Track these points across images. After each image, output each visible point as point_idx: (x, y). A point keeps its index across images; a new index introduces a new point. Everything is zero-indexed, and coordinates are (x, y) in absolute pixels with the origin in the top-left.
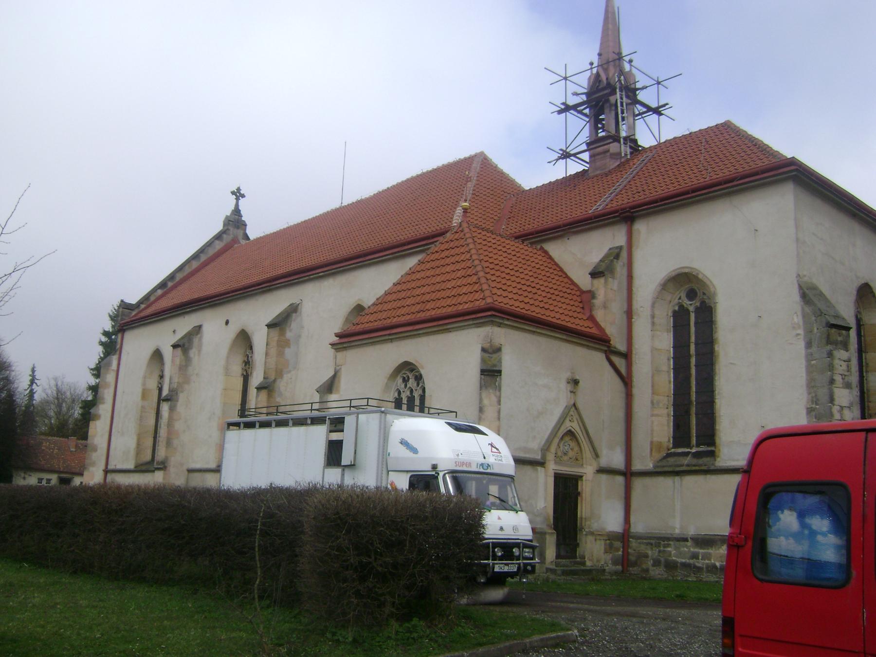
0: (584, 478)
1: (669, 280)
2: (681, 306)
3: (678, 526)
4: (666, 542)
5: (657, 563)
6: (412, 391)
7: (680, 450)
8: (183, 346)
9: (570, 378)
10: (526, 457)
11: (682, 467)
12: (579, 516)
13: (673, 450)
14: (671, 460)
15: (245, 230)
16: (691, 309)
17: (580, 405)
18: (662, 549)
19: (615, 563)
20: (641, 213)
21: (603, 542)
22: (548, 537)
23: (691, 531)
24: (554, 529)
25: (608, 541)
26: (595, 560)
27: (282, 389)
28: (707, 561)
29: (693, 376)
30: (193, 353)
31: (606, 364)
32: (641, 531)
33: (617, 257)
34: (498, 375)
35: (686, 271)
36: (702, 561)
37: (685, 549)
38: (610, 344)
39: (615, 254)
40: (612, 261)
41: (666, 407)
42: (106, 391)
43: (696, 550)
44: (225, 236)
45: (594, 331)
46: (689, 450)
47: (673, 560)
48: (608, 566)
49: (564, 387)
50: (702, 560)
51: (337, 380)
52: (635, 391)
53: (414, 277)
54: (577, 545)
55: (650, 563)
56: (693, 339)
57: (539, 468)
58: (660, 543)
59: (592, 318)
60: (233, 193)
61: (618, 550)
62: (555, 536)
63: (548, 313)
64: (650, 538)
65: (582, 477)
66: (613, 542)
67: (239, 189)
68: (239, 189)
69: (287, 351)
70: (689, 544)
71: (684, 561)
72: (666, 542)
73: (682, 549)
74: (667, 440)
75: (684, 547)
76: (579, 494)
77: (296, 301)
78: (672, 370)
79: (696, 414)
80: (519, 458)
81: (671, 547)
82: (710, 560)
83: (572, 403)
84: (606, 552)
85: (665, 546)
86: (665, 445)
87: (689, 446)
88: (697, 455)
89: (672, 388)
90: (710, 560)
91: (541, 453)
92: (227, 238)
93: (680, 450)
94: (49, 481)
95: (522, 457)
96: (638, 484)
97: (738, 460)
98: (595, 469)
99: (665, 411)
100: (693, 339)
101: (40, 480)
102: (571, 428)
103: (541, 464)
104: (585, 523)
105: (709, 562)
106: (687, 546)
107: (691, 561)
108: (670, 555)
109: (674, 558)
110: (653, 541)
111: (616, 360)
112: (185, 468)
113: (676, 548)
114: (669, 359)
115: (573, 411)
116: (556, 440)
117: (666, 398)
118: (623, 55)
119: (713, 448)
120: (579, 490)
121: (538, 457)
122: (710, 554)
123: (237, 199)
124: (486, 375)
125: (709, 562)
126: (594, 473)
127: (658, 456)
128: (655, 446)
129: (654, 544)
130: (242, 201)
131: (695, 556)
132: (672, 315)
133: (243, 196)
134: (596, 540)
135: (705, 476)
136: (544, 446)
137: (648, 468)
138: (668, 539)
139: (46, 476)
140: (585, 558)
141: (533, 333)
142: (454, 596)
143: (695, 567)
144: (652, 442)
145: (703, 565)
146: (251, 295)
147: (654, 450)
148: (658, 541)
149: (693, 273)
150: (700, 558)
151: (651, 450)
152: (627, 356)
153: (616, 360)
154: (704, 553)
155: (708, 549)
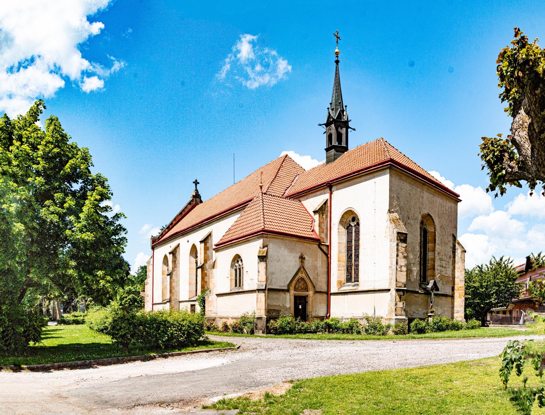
8: (174, 253)
15: (200, 198)
30: (177, 254)
31: (319, 250)
42: (150, 273)
44: (192, 202)
49: (298, 260)
53: (238, 223)
60: (194, 182)
68: (196, 180)
87: (351, 282)
96: (325, 296)
103: (288, 291)
112: (178, 300)
116: (294, 282)
121: (286, 288)
130: (198, 185)
133: (198, 183)
142: (76, 276)
146: (352, 179)
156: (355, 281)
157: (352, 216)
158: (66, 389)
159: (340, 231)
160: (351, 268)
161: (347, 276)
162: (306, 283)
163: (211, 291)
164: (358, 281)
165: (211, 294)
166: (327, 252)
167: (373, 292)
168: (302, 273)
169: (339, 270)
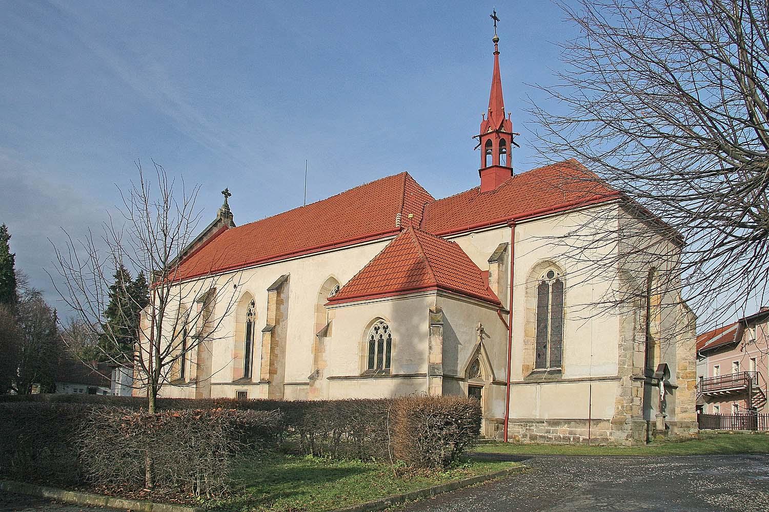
2: (544, 282)
6: (381, 336)
7: (540, 370)
13: (535, 370)
14: (535, 376)
16: (550, 283)
18: (528, 428)
23: (546, 417)
27: (280, 331)
33: (505, 250)
39: (503, 248)
40: (502, 253)
45: (490, 297)
56: (550, 302)
59: (488, 289)
63: (465, 286)
67: (227, 190)
69: (282, 307)
70: (545, 424)
71: (541, 434)
77: (286, 273)
86: (530, 367)
87: (545, 367)
88: (550, 373)
92: (220, 225)
93: (540, 370)
94: (81, 391)
97: (576, 375)
100: (550, 302)
101: (75, 390)
107: (546, 435)
118: (614, 386)
119: (560, 369)
123: (226, 197)
128: (526, 368)
131: (548, 432)
133: (230, 195)
139: (78, 387)
141: (459, 300)
152: (509, 313)
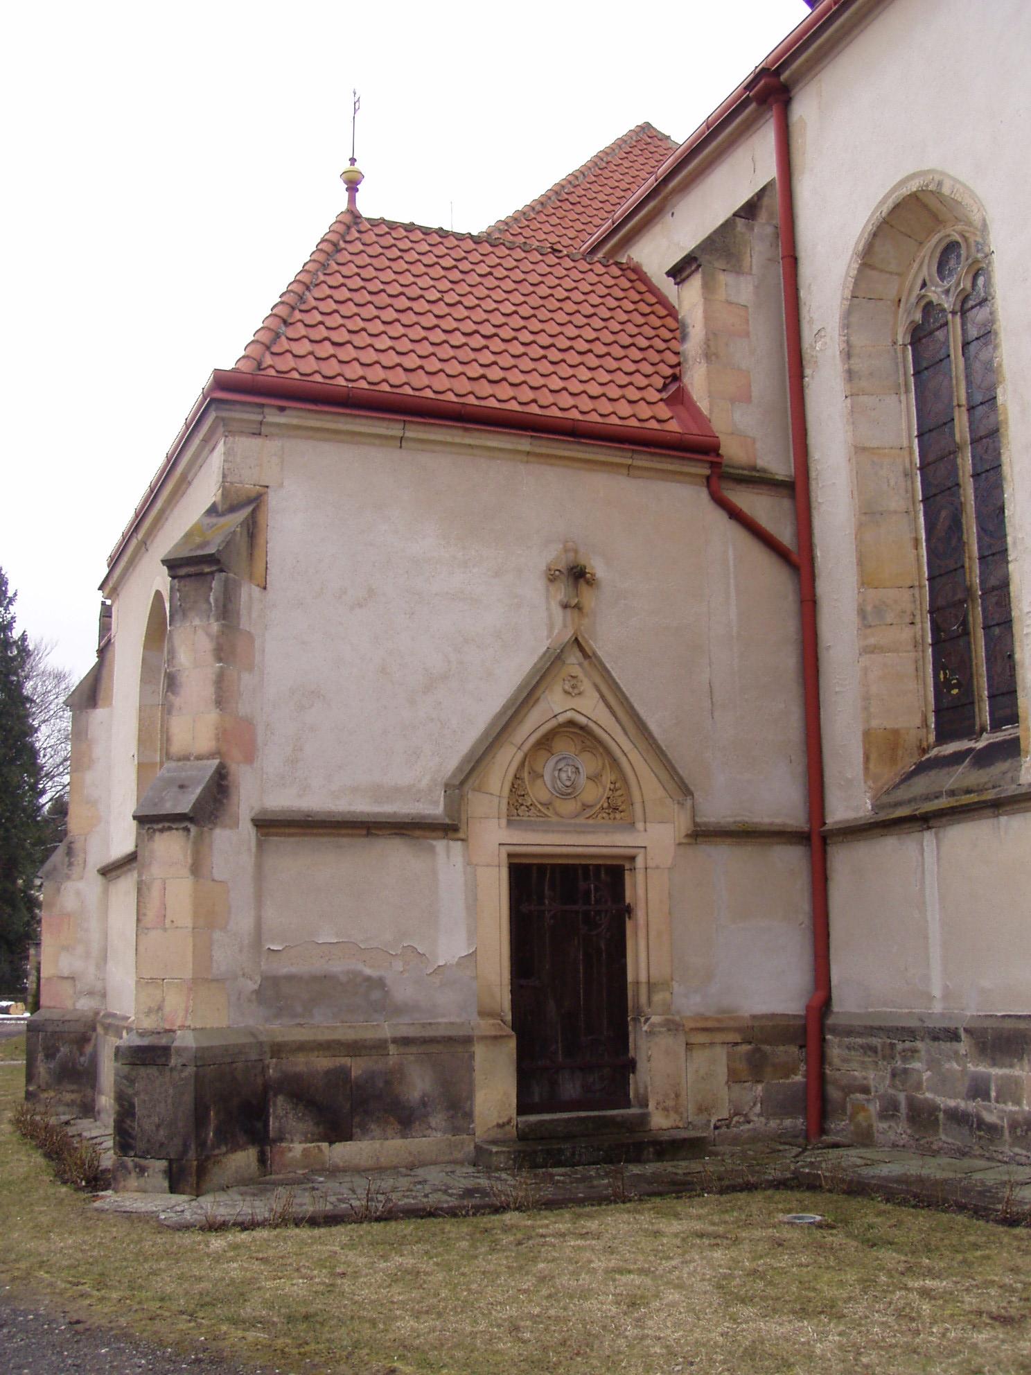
0: (640, 862)
1: (875, 235)
3: (937, 992)
4: (908, 1044)
5: (889, 1110)
9: (562, 566)
10: (378, 814)
11: (936, 801)
12: (630, 978)
17: (603, 647)
18: (899, 1064)
19: (778, 1106)
20: (794, 66)
21: (721, 1054)
22: (479, 1051)
23: (971, 1008)
24: (513, 1029)
25: (745, 1048)
26: (691, 1108)
28: (1011, 1107)
29: (968, 507)
31: (718, 517)
32: (854, 1010)
34: (212, 573)
35: (913, 186)
36: (1001, 1106)
37: (955, 1066)
38: (718, 455)
41: (908, 620)
43: (982, 1069)
46: (972, 744)
47: (926, 1100)
48: (749, 1122)
50: (997, 1102)
51: (105, 673)
52: (824, 587)
54: (631, 1066)
55: (874, 1108)
57: (440, 845)
58: (892, 1046)
61: (790, 1070)
62: (513, 1044)
64: (871, 1031)
65: (632, 858)
66: (767, 1048)
70: (963, 1047)
72: (908, 1044)
73: (947, 1066)
74: (917, 721)
75: (949, 1059)
76: (628, 910)
78: (921, 506)
79: (983, 628)
80: (847, 825)
81: (919, 1060)
82: (1018, 1102)
83: (568, 635)
84: (734, 1078)
85: (905, 1059)
86: (911, 738)
89: (925, 559)
90: (1018, 1102)
91: (445, 797)
95: (362, 813)
96: (792, 858)
98: (683, 833)
99: (906, 634)
102: (569, 715)
103: (448, 829)
104: (649, 998)
105: (1016, 1108)
106: (956, 1056)
108: (918, 1086)
109: (929, 1095)
110: (876, 1041)
111: (747, 500)
113: (933, 1064)
114: (907, 475)
115: (580, 665)
116: (507, 760)
117: (906, 594)
120: (627, 901)
121: (435, 809)
122: (1017, 1082)
124: (189, 576)
125: (1016, 1108)
126: (680, 844)
127: (889, 775)
129: (879, 1048)
131: (979, 1090)
132: (908, 340)
134: (689, 1046)
135: (994, 821)
136: (454, 775)
137: (861, 814)
138: (910, 1033)
140: (647, 1106)
143: (981, 1124)
144: (867, 734)
145: (1002, 1119)
147: (873, 756)
148: (889, 1041)
149: (930, 188)
150: (993, 1094)
151: (867, 758)
153: (747, 500)
154: (1002, 1077)
155: (1011, 1066)
156: (996, 726)
157: (934, 243)
158: (212, 1205)
159: (856, 364)
160: (965, 623)
161: (940, 689)
162: (615, 763)
163: (77, 846)
164: (1014, 719)
165: (76, 871)
166: (785, 534)
167: (391, 428)
168: (573, 691)
169: (868, 650)
